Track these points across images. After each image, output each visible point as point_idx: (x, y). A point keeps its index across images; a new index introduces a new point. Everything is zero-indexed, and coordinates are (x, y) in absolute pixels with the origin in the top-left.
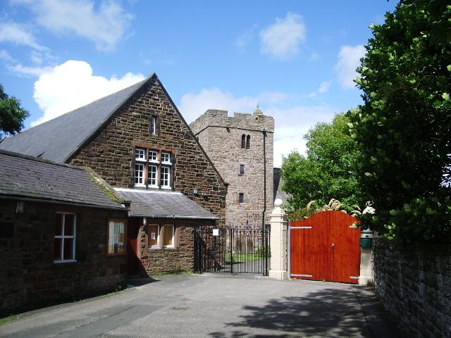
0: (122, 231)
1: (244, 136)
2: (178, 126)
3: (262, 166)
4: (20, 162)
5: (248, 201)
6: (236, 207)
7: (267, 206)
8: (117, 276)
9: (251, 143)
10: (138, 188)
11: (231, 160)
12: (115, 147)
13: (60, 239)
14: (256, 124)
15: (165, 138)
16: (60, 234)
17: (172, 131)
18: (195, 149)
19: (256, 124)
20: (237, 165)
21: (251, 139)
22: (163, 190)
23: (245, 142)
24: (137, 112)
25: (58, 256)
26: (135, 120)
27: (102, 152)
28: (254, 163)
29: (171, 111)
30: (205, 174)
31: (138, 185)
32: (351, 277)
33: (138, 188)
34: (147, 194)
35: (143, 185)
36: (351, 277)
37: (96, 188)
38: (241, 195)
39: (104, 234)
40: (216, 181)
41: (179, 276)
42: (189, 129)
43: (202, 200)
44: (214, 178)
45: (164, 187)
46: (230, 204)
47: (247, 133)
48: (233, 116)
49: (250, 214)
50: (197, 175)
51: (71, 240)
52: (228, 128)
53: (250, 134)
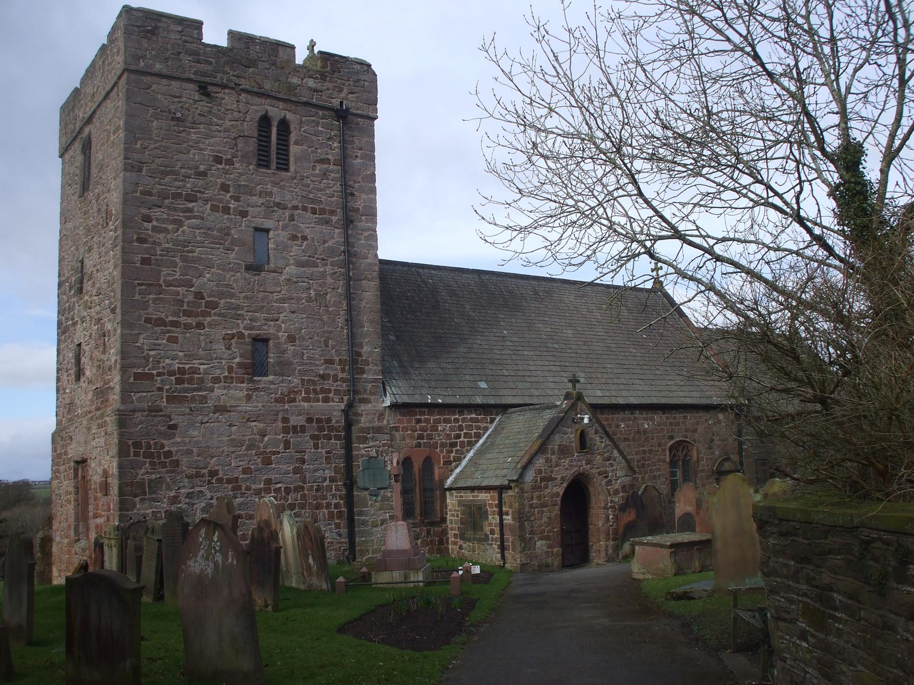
1: (265, 121)
3: (337, 235)
5: (284, 368)
6: (238, 392)
9: (294, 149)
11: (214, 208)
20: (241, 229)
28: (308, 225)
38: (261, 341)
39: (69, 225)
41: (77, 187)
46: (216, 380)
47: (276, 112)
48: (223, 42)
49: (297, 420)
52: (203, 89)
53: (289, 116)
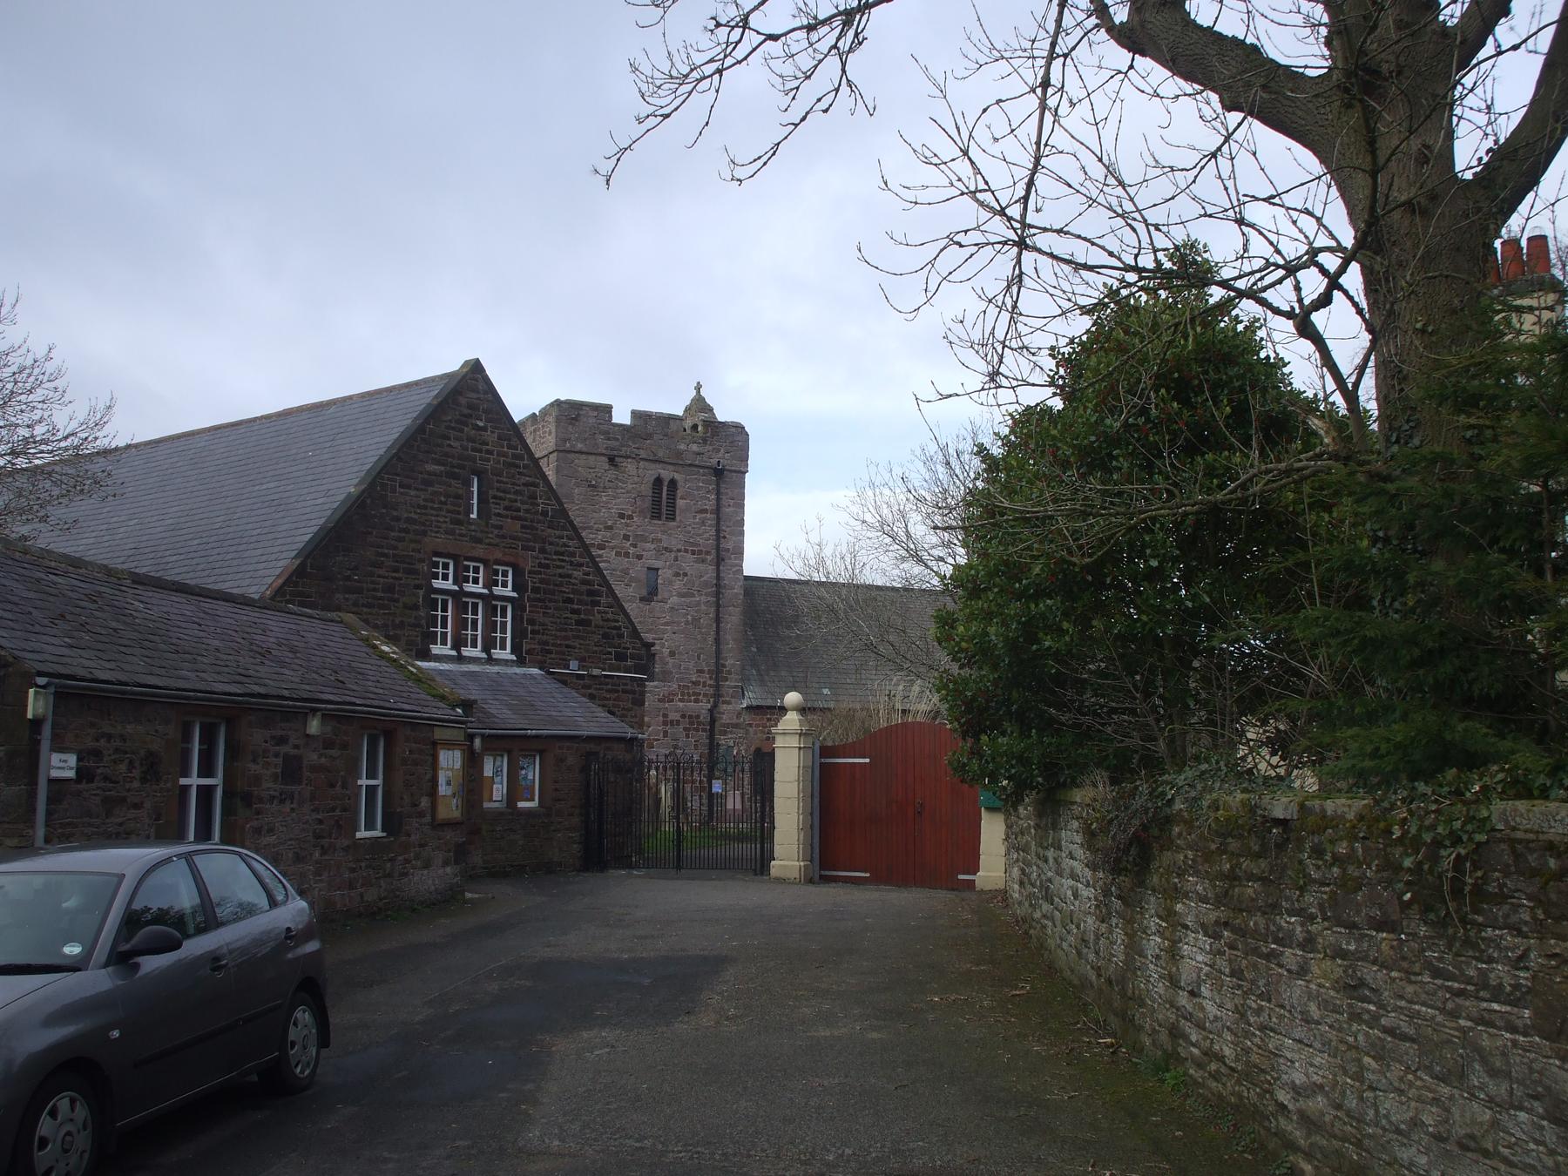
0: (458, 765)
1: (658, 481)
2: (533, 497)
3: (709, 572)
4: (207, 605)
7: (723, 691)
8: (448, 870)
9: (680, 503)
10: (438, 658)
12: (385, 555)
13: (187, 788)
14: (695, 447)
15: (501, 527)
16: (186, 774)
17: (518, 510)
18: (573, 554)
19: (695, 447)
21: (679, 493)
22: (498, 662)
23: (662, 501)
24: (439, 463)
25: (356, 829)
26: (430, 484)
27: (356, 568)
28: (688, 564)
29: (515, 456)
30: (596, 619)
31: (436, 649)
32: (961, 877)
33: (438, 658)
34: (464, 674)
35: (447, 650)
36: (961, 877)
37: (343, 656)
40: (621, 636)
42: (561, 504)
43: (589, 687)
44: (619, 628)
45: (497, 653)
47: (667, 474)
49: (674, 716)
50: (579, 623)
51: (375, 787)
53: (677, 476)
